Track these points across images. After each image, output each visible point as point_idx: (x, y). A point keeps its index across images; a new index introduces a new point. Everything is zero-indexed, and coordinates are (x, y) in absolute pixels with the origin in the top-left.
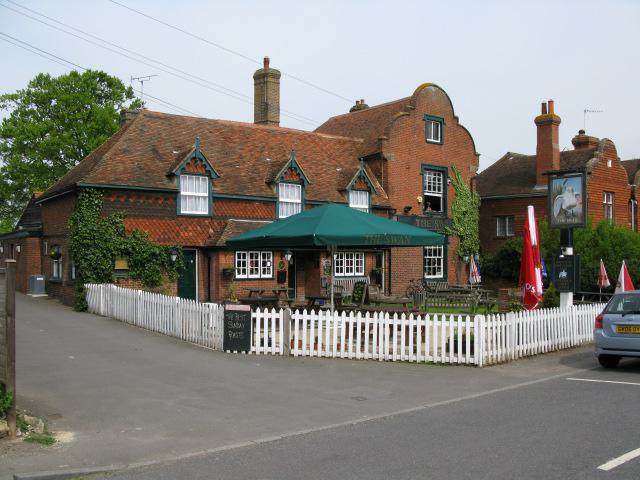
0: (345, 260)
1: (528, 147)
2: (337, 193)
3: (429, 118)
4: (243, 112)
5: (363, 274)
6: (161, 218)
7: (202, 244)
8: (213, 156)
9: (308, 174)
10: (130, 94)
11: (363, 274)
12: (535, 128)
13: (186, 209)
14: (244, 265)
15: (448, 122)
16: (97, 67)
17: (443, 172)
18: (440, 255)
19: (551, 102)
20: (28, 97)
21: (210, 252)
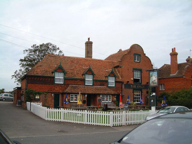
0: (105, 97)
1: (169, 63)
2: (104, 78)
3: (135, 54)
4: (81, 54)
5: (111, 101)
6: (49, 84)
7: (61, 92)
8: (66, 67)
9: (95, 73)
10: (58, 49)
11: (111, 101)
12: (170, 56)
13: (155, 95)
14: (73, 98)
15: (142, 56)
16: (136, 43)
17: (140, 71)
18: (139, 96)
19: (175, 48)
20: (31, 51)
21: (63, 94)
